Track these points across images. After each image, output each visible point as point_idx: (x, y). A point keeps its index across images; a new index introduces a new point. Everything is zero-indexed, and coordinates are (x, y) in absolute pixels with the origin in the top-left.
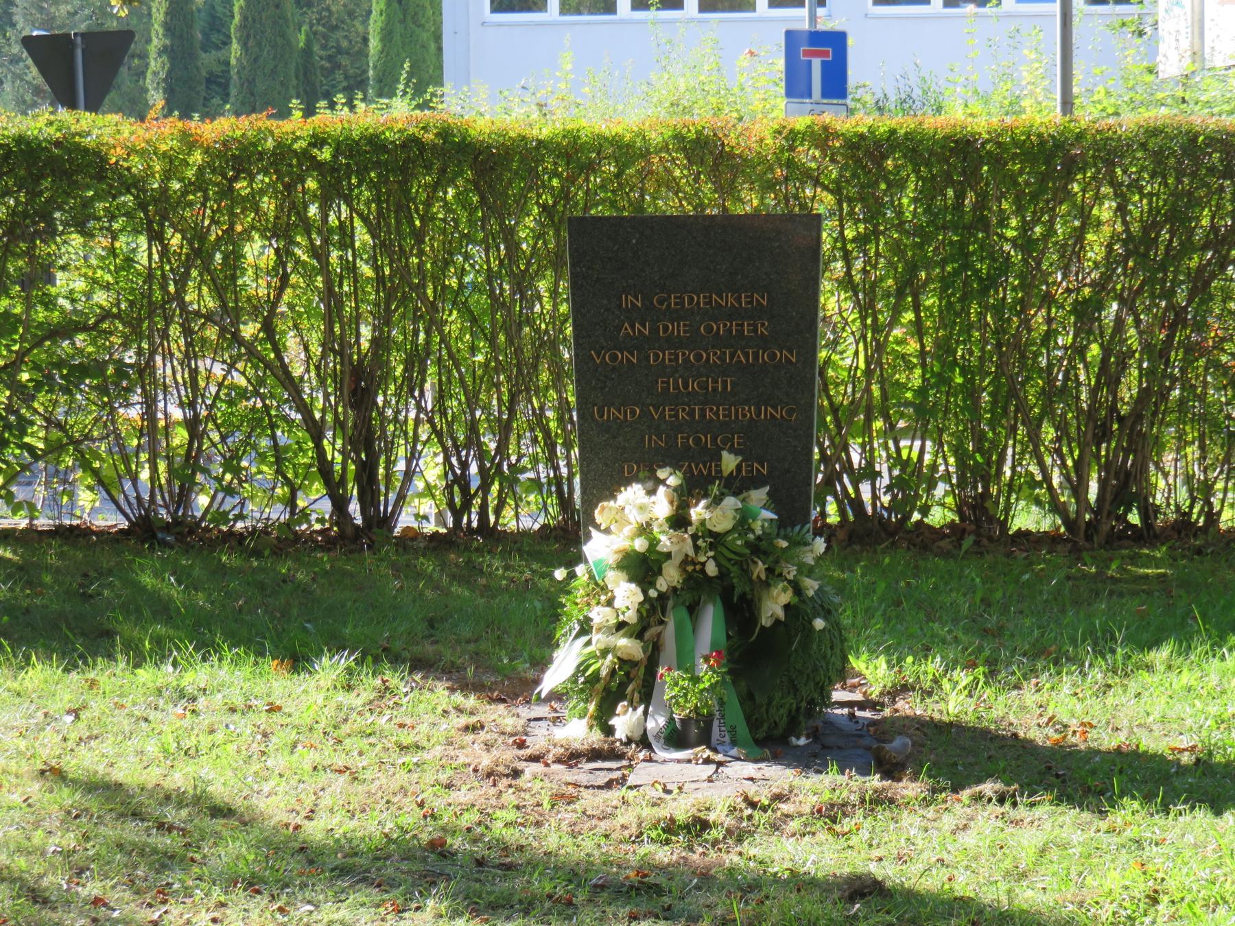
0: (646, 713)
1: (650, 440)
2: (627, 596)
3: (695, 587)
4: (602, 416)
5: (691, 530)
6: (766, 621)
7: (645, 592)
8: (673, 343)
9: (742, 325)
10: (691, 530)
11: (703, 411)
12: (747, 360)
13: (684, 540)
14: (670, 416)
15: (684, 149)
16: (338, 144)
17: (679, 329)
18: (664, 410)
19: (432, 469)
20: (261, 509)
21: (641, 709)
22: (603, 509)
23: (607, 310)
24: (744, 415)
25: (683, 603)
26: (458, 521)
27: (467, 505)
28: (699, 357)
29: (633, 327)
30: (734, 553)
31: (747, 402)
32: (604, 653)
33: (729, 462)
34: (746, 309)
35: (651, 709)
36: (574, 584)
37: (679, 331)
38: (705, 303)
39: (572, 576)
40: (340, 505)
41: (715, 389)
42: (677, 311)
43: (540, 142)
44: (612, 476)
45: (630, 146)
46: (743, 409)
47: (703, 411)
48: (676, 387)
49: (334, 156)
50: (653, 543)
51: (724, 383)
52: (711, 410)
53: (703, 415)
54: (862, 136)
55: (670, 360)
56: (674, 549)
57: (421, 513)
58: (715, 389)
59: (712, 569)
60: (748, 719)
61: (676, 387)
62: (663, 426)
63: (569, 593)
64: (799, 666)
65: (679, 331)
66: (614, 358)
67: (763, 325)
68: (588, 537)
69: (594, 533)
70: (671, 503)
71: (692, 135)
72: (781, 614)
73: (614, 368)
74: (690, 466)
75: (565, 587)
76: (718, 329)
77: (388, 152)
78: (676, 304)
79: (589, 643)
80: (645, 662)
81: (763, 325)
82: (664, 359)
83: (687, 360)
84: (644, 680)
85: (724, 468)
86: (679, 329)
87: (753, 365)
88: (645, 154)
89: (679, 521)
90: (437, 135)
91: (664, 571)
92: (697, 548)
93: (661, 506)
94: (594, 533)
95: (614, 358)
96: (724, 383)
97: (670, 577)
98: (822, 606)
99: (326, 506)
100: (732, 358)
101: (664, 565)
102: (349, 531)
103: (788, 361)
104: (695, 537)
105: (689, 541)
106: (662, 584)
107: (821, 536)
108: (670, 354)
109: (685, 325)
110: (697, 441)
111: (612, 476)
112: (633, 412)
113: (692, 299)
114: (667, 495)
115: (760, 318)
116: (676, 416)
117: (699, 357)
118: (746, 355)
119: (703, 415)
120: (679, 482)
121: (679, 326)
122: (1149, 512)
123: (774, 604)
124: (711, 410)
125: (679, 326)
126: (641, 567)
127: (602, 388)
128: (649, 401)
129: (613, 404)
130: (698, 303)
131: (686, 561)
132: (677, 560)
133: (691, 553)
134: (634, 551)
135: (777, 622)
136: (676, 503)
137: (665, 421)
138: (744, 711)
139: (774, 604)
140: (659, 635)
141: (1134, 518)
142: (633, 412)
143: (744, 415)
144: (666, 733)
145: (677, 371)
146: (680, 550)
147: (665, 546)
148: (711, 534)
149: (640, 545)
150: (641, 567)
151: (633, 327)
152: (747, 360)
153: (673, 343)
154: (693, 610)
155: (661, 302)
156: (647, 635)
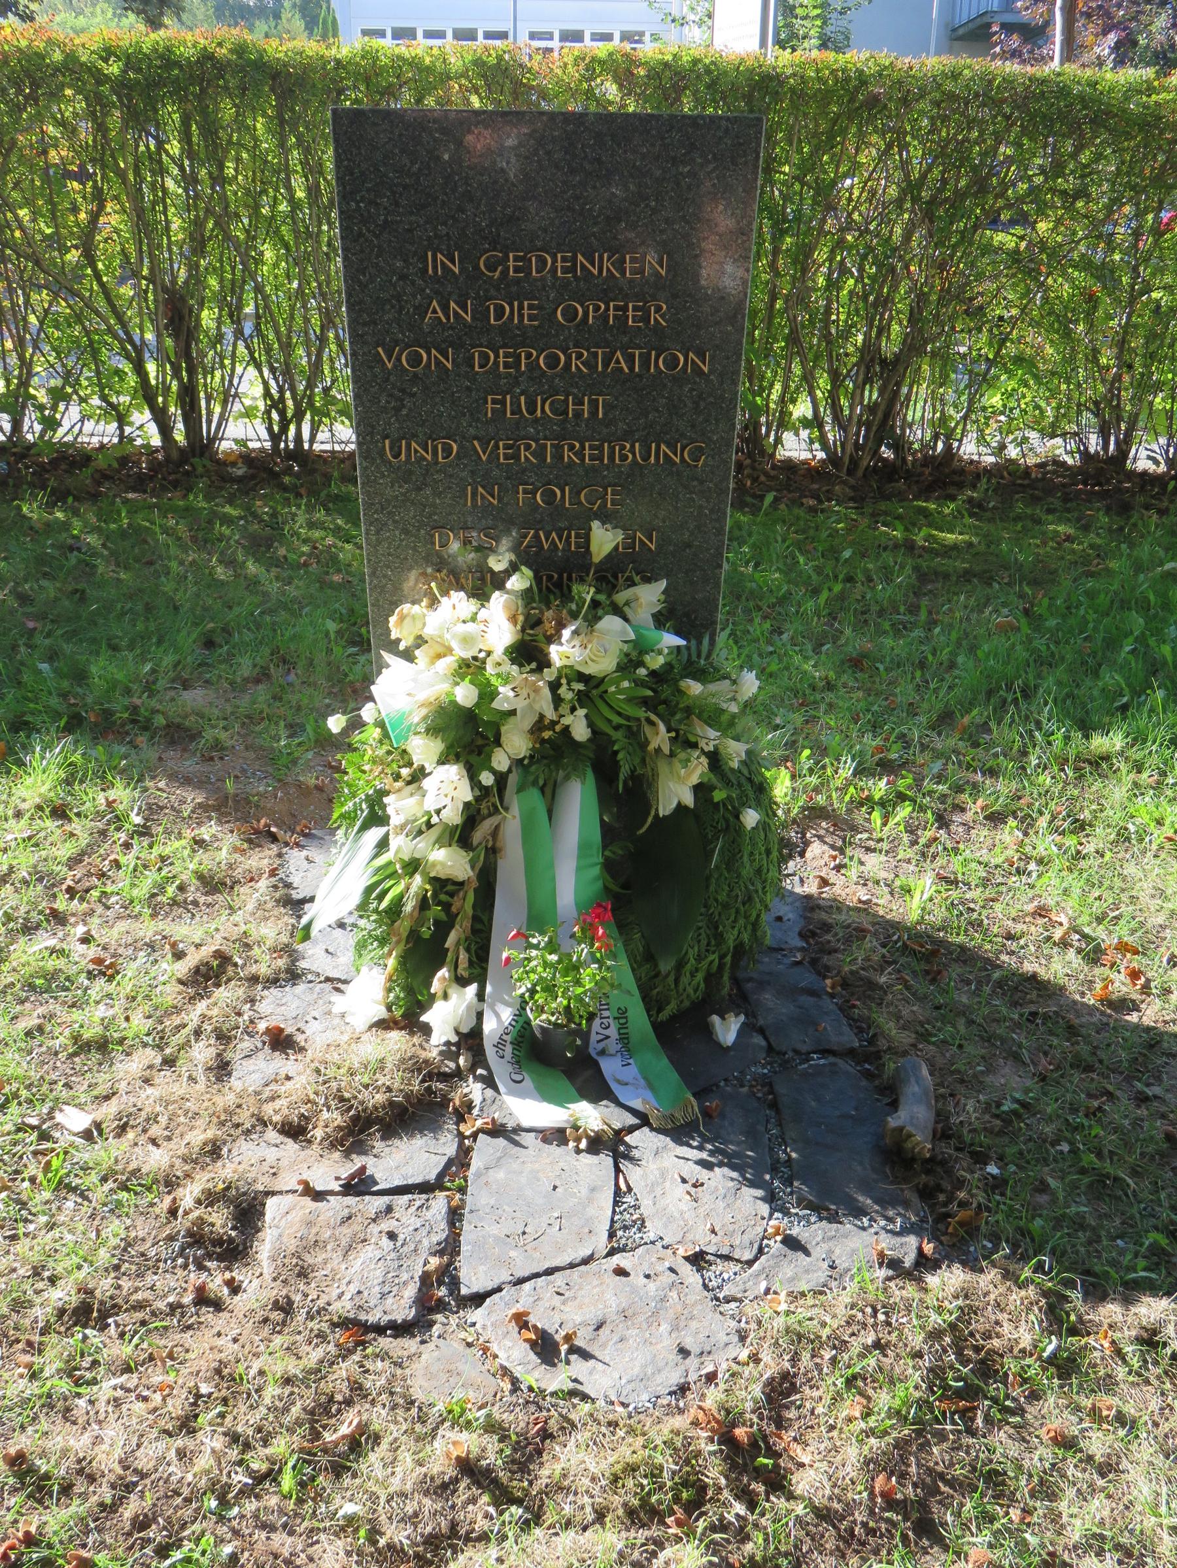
0: (481, 996)
1: (474, 494)
2: (447, 789)
3: (552, 753)
4: (397, 455)
5: (549, 674)
6: (665, 807)
7: (472, 774)
8: (511, 337)
9: (625, 309)
10: (549, 674)
11: (558, 449)
12: (632, 368)
13: (537, 690)
14: (506, 457)
15: (484, 76)
16: (128, 57)
17: (523, 314)
18: (497, 447)
19: (251, 386)
20: (99, 433)
21: (472, 989)
22: (402, 618)
23: (403, 277)
24: (624, 458)
25: (535, 783)
26: (275, 445)
27: (284, 429)
28: (553, 361)
29: (445, 308)
30: (619, 714)
31: (627, 435)
32: (413, 866)
33: (604, 540)
34: (631, 281)
35: (489, 989)
36: (356, 737)
37: (521, 316)
38: (565, 270)
39: (356, 724)
40: (165, 430)
41: (578, 415)
42: (518, 282)
43: (338, 62)
44: (415, 549)
45: (429, 70)
46: (623, 448)
47: (558, 449)
48: (517, 410)
49: (125, 72)
50: (487, 694)
51: (594, 404)
52: (572, 448)
53: (558, 456)
54: (666, 65)
55: (506, 366)
56: (520, 704)
57: (242, 431)
58: (578, 415)
59: (581, 732)
60: (645, 998)
61: (517, 410)
62: (496, 473)
63: (351, 748)
64: (722, 897)
65: (521, 316)
66: (415, 360)
67: (658, 309)
68: (382, 666)
69: (387, 657)
70: (513, 619)
71: (492, 61)
72: (689, 800)
73: (415, 375)
74: (536, 536)
75: (342, 743)
76: (586, 313)
77: (181, 67)
78: (517, 270)
79: (383, 844)
80: (475, 884)
81: (658, 309)
82: (496, 363)
83: (533, 366)
84: (475, 918)
85: (594, 548)
86: (523, 314)
87: (639, 376)
88: (445, 77)
89: (528, 653)
90: (231, 51)
91: (503, 739)
92: (557, 701)
93: (495, 625)
94: (387, 657)
95: (415, 360)
96: (594, 404)
97: (516, 743)
98: (750, 780)
99: (152, 429)
100: (606, 365)
101: (503, 729)
102: (175, 455)
103: (698, 371)
104: (554, 686)
105: (547, 692)
106: (501, 761)
107: (751, 669)
108: (506, 356)
109: (531, 307)
110: (549, 497)
111: (415, 549)
112: (447, 450)
113: (545, 262)
114: (506, 607)
115: (654, 299)
116: (516, 457)
117: (553, 361)
118: (630, 360)
119: (558, 456)
120: (526, 584)
121: (521, 308)
122: (899, 445)
123: (676, 789)
124: (572, 448)
125: (521, 308)
126: (467, 734)
127: (397, 410)
128: (472, 431)
129: (414, 436)
130: (554, 270)
131: (540, 725)
132: (528, 722)
133: (550, 714)
134: (454, 703)
135: (681, 808)
136: (521, 618)
137: (499, 465)
138: (638, 980)
139: (676, 789)
140: (497, 828)
141: (887, 453)
142: (447, 450)
143: (624, 458)
144: (514, 1033)
145: (518, 384)
146: (530, 706)
147: (507, 699)
148: (582, 677)
149: (465, 694)
150: (467, 734)
151: (445, 308)
152: (632, 368)
153: (511, 337)
154: (551, 793)
155: (491, 267)
156: (478, 836)
